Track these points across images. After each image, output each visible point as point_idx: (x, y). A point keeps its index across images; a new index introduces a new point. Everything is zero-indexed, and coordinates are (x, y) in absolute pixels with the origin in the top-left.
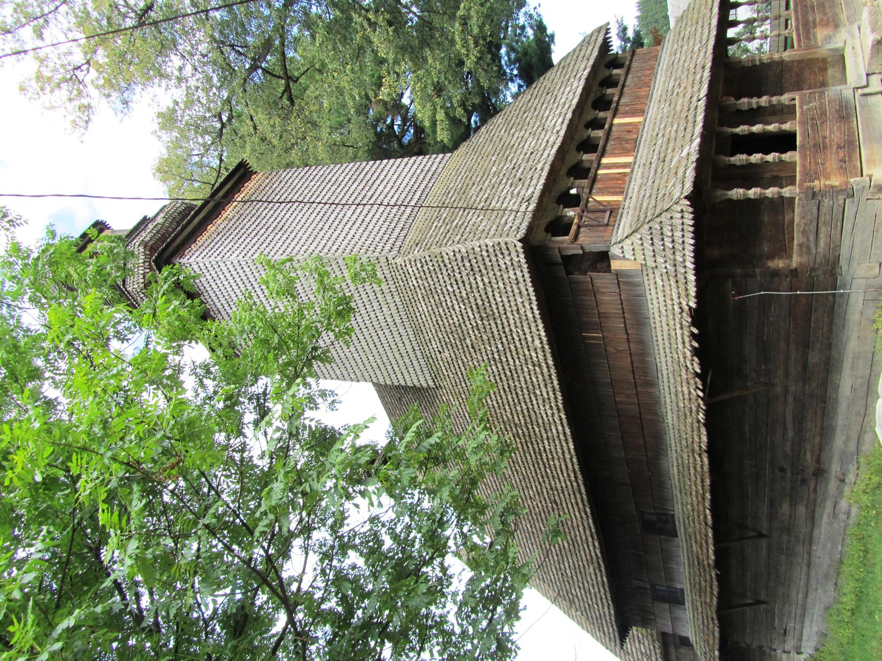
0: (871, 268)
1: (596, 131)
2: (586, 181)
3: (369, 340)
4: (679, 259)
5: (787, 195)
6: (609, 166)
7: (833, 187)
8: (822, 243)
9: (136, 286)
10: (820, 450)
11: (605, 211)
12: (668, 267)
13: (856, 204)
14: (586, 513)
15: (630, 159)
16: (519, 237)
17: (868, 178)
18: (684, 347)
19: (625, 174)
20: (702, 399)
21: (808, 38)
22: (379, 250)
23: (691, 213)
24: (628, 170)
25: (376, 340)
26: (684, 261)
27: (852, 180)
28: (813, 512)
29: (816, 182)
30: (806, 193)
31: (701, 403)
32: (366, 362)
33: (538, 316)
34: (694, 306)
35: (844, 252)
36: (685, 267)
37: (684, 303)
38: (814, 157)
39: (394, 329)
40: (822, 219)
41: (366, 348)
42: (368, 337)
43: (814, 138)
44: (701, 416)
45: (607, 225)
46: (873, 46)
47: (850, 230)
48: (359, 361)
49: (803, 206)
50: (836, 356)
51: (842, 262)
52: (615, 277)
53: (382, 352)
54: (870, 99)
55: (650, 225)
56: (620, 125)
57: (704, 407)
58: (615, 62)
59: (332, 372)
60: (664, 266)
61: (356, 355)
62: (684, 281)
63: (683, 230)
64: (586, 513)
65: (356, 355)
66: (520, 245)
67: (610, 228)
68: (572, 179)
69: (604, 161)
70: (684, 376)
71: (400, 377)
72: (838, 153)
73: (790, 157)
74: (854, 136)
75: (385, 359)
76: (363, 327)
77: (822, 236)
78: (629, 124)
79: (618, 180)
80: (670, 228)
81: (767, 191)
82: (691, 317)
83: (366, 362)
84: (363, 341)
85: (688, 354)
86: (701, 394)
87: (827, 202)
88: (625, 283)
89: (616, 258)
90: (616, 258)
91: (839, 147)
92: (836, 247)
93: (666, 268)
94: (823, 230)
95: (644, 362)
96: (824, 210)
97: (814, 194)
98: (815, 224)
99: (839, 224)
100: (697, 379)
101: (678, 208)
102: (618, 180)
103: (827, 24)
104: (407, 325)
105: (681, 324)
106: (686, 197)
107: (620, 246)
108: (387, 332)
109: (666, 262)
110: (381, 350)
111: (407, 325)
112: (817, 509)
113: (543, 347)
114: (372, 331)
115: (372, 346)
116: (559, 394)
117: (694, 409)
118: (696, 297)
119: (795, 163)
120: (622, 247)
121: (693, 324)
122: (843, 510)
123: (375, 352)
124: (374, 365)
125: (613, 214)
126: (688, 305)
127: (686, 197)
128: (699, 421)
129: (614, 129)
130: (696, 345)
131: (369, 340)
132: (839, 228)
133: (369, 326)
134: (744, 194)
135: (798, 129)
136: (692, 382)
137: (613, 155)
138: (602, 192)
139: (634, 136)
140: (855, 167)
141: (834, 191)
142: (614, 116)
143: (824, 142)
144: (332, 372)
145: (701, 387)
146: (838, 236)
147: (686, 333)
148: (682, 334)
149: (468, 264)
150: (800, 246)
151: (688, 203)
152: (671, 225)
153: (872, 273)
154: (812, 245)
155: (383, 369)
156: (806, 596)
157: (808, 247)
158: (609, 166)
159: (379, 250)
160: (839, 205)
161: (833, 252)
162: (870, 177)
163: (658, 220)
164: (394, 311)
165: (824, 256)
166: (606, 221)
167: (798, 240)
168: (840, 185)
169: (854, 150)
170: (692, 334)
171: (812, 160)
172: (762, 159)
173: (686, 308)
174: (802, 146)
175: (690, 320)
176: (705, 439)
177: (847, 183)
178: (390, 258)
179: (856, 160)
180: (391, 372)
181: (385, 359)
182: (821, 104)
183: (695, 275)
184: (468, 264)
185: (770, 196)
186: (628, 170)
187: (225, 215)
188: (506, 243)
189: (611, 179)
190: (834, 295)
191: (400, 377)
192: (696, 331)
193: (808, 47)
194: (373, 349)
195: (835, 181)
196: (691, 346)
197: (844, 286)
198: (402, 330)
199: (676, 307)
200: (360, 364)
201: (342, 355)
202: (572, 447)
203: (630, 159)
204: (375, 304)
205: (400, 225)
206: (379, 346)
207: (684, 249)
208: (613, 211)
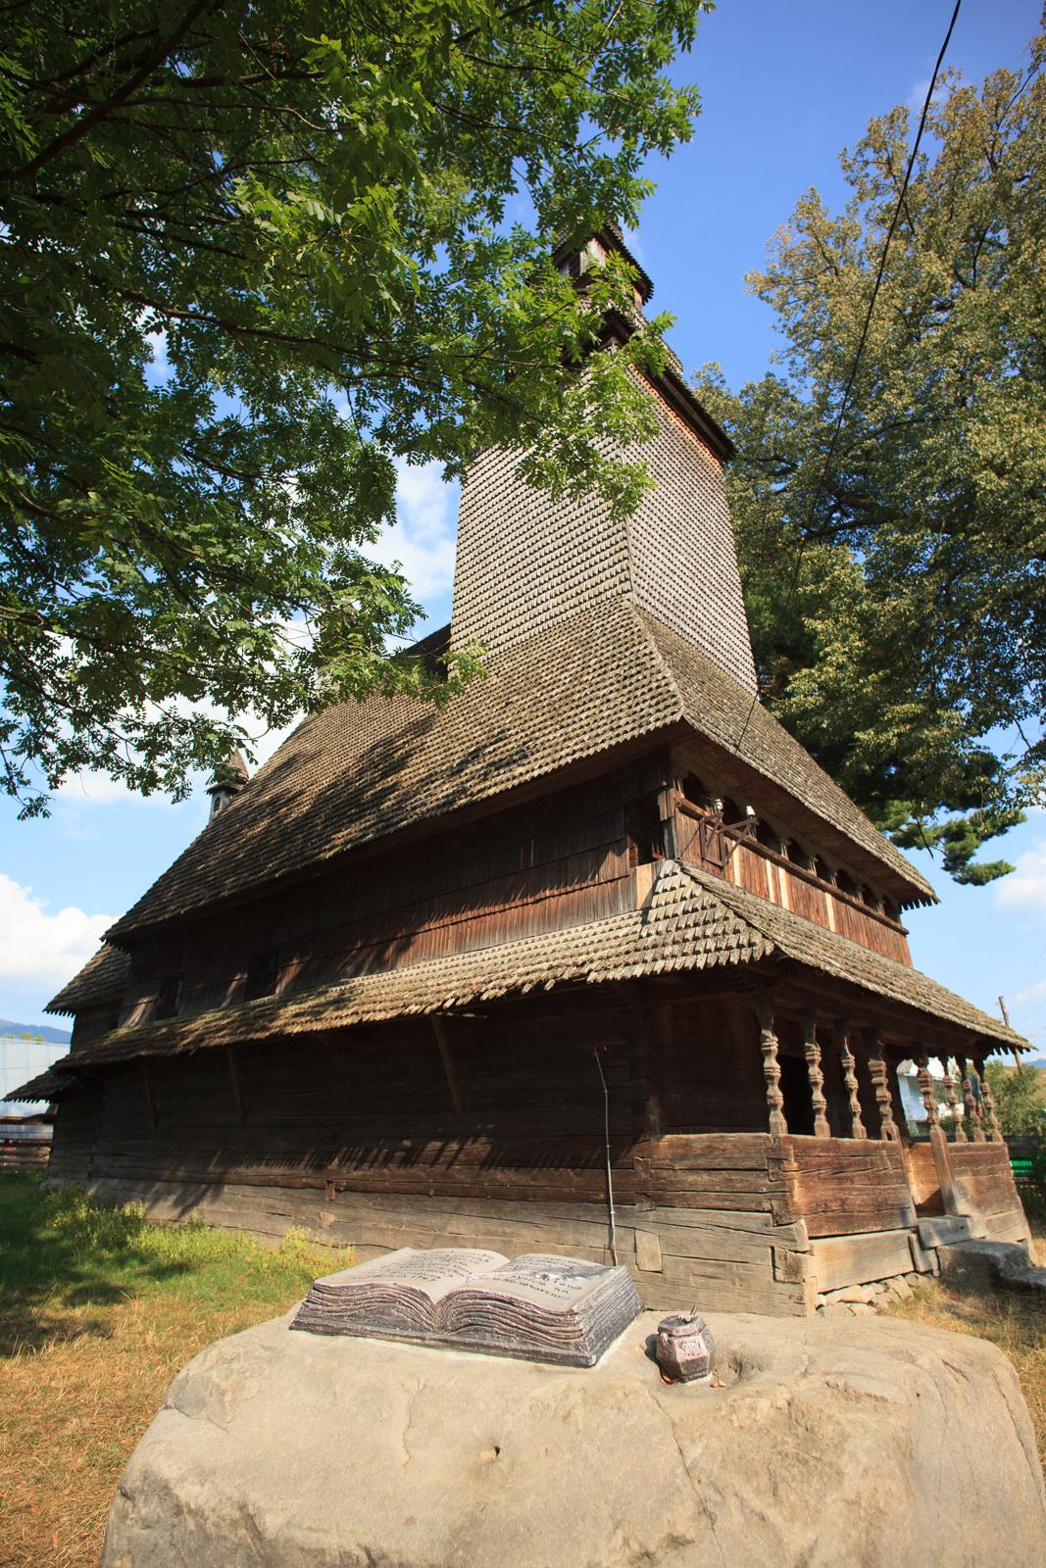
0: (653, 1258)
3: (512, 588)
4: (668, 951)
5: (772, 1119)
6: (775, 875)
7: (791, 1191)
8: (691, 1178)
10: (365, 1191)
12: (650, 939)
13: (764, 1230)
16: (687, 717)
17: (807, 1248)
18: (520, 975)
19: (767, 896)
20: (440, 1008)
21: (961, 1163)
22: (639, 581)
23: (752, 958)
25: (511, 597)
26: (663, 958)
27: (803, 1222)
28: (276, 1185)
29: (795, 1165)
30: (779, 1148)
31: (435, 1006)
32: (481, 589)
33: (563, 762)
34: (591, 978)
35: (679, 1214)
36: (655, 960)
37: (593, 966)
38: (827, 1164)
39: (527, 616)
40: (735, 1176)
41: (502, 585)
42: (516, 585)
43: (850, 1165)
44: (414, 1008)
46: (986, 1257)
47: (717, 1221)
48: (483, 580)
49: (755, 1145)
51: (662, 1212)
52: (623, 874)
53: (495, 607)
54: (905, 1253)
55: (719, 904)
56: (824, 900)
57: (427, 1011)
58: (893, 912)
59: (464, 576)
60: (653, 932)
61: (490, 576)
62: (631, 961)
63: (718, 949)
65: (490, 576)
66: (677, 717)
67: (699, 862)
69: (782, 872)
70: (474, 981)
71: (461, 634)
72: (836, 1200)
73: (820, 1126)
74: (859, 1227)
75: (486, 611)
76: (530, 577)
77: (705, 1177)
78: (826, 914)
79: (761, 885)
80: (720, 931)
81: (776, 1087)
82: (570, 979)
83: (481, 589)
84: (510, 580)
85: (510, 981)
86: (448, 1004)
87: (764, 1182)
88: (615, 891)
89: (656, 869)
90: (656, 869)
91: (843, 1202)
92: (685, 1199)
93: (649, 935)
94: (717, 1177)
95: (493, 929)
96: (751, 1177)
97: (779, 1161)
98: (725, 1165)
99: (727, 1204)
100: (470, 997)
101: (757, 938)
102: (761, 885)
103: (979, 1192)
104: (536, 630)
105: (558, 966)
106: (777, 948)
107: (678, 870)
108: (524, 608)
109: (658, 933)
110: (498, 605)
111: (536, 630)
112: (279, 1190)
113: (514, 778)
114: (524, 589)
115: (504, 593)
117: (425, 998)
118: (605, 981)
119: (812, 1133)
120: (675, 874)
121: (560, 984)
122: (278, 1227)
123: (496, 597)
124: (478, 600)
125: (717, 870)
126: (590, 971)
127: (777, 948)
128: (405, 1006)
130: (526, 989)
131: (512, 588)
132: (720, 1204)
133: (532, 585)
134: (769, 1052)
135: (857, 1140)
136: (466, 990)
137: (790, 885)
138: (744, 860)
140: (820, 1227)
141: (783, 1192)
142: (834, 895)
143: (847, 1178)
144: (464, 576)
145: (459, 1003)
146: (706, 1203)
147: (543, 975)
148: (541, 970)
149: (633, 671)
150: (687, 1144)
151: (768, 952)
152: (724, 933)
153: (646, 1259)
154: (688, 1163)
155: (472, 611)
156: (516, 1354)
157: (683, 1157)
158: (775, 875)
159: (639, 581)
160: (760, 1203)
161: (677, 1196)
162: (810, 1252)
163: (731, 914)
164: (552, 612)
165: (672, 1183)
167: (695, 1141)
168: (794, 1204)
169: (841, 1225)
170: (541, 984)
171: (823, 1160)
172: (816, 1084)
173: (585, 970)
174: (838, 1146)
175: (566, 977)
176: (379, 1016)
177: (797, 1214)
178: (629, 595)
179: (829, 1229)
180: (467, 623)
181: (486, 611)
182: (891, 1177)
183: (643, 975)
184: (633, 671)
185: (770, 1092)
187: (672, 414)
188: (675, 704)
189: (760, 877)
191: (461, 634)
192: (549, 986)
193: (951, 1161)
194: (500, 595)
195: (799, 1195)
196: (523, 984)
197: (621, 1215)
199: (584, 957)
200: (479, 583)
201: (491, 559)
204: (562, 588)
205: (671, 616)
206: (503, 602)
207: (684, 954)
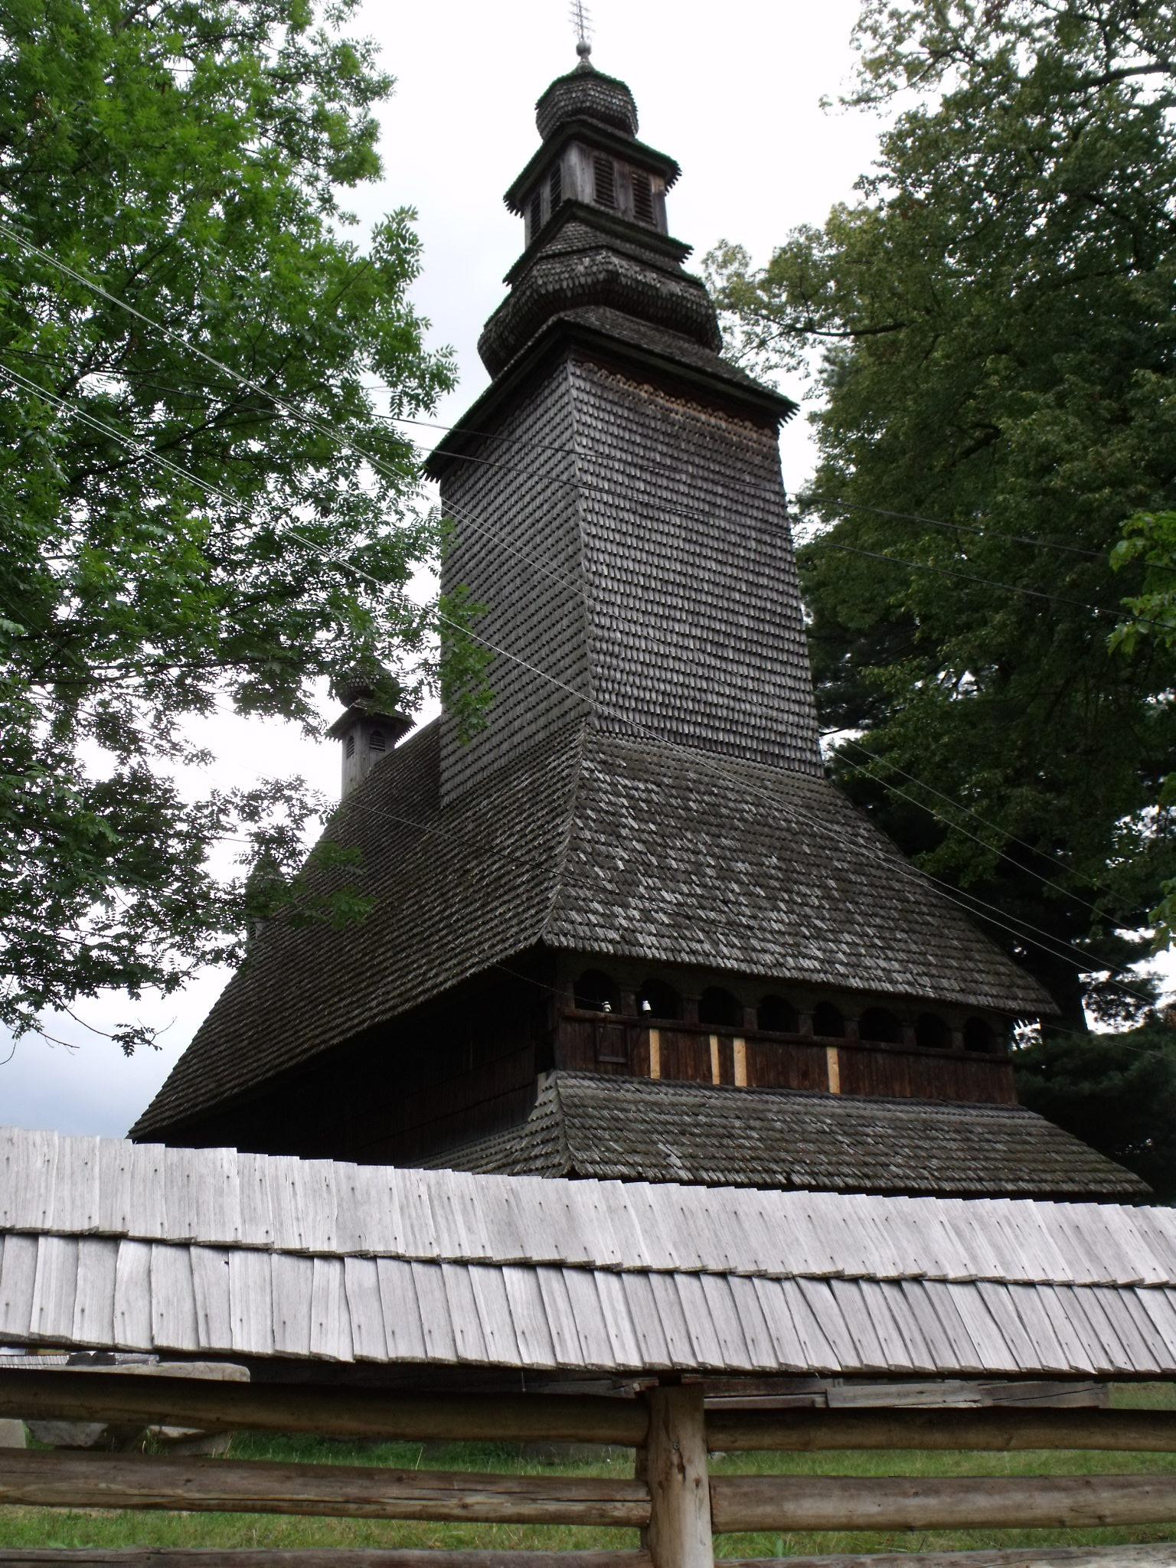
1: (810, 1022)
2: (696, 1019)
9: (540, 282)
11: (625, 1055)
14: (268, 1071)
15: (740, 1078)
24: (716, 1081)
45: (597, 1062)
50: (1161, 1556)
64: (268, 1071)
66: (534, 940)
67: (591, 1066)
68: (699, 998)
79: (696, 1068)
116: (389, 1015)
129: (815, 1050)
139: (794, 1083)
166: (601, 1058)
186: (716, 1081)
190: (520, 1381)
198: (505, 746)
202: (335, 1041)
203: (740, 1078)
208: (632, 1066)
